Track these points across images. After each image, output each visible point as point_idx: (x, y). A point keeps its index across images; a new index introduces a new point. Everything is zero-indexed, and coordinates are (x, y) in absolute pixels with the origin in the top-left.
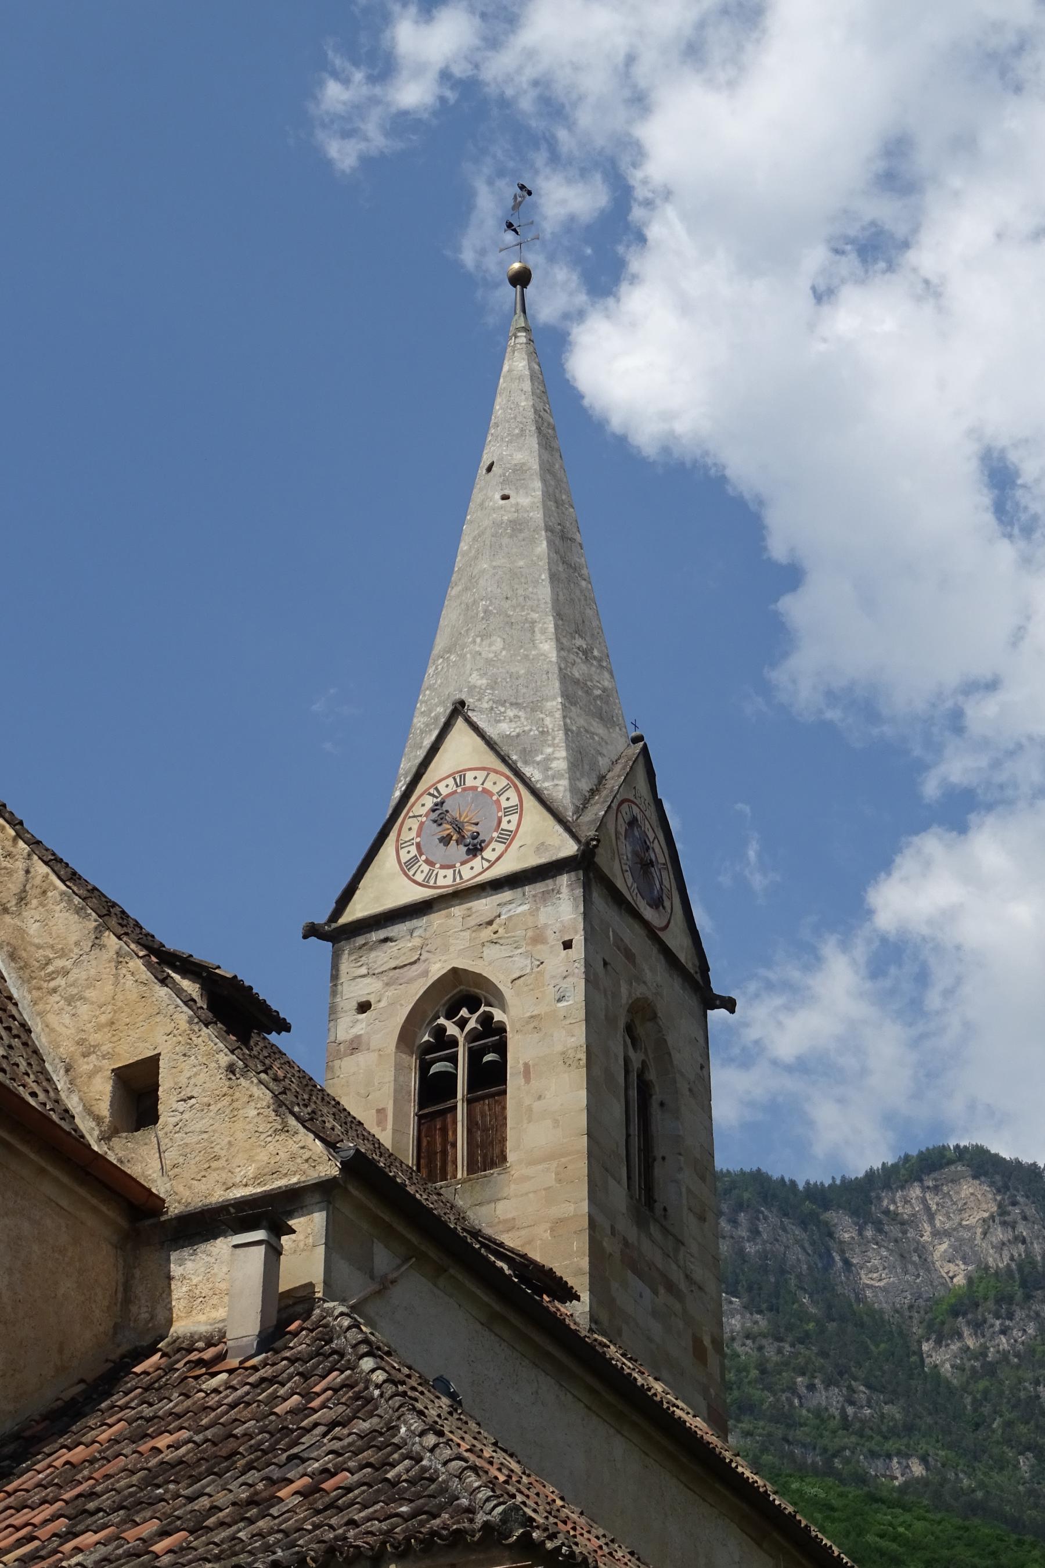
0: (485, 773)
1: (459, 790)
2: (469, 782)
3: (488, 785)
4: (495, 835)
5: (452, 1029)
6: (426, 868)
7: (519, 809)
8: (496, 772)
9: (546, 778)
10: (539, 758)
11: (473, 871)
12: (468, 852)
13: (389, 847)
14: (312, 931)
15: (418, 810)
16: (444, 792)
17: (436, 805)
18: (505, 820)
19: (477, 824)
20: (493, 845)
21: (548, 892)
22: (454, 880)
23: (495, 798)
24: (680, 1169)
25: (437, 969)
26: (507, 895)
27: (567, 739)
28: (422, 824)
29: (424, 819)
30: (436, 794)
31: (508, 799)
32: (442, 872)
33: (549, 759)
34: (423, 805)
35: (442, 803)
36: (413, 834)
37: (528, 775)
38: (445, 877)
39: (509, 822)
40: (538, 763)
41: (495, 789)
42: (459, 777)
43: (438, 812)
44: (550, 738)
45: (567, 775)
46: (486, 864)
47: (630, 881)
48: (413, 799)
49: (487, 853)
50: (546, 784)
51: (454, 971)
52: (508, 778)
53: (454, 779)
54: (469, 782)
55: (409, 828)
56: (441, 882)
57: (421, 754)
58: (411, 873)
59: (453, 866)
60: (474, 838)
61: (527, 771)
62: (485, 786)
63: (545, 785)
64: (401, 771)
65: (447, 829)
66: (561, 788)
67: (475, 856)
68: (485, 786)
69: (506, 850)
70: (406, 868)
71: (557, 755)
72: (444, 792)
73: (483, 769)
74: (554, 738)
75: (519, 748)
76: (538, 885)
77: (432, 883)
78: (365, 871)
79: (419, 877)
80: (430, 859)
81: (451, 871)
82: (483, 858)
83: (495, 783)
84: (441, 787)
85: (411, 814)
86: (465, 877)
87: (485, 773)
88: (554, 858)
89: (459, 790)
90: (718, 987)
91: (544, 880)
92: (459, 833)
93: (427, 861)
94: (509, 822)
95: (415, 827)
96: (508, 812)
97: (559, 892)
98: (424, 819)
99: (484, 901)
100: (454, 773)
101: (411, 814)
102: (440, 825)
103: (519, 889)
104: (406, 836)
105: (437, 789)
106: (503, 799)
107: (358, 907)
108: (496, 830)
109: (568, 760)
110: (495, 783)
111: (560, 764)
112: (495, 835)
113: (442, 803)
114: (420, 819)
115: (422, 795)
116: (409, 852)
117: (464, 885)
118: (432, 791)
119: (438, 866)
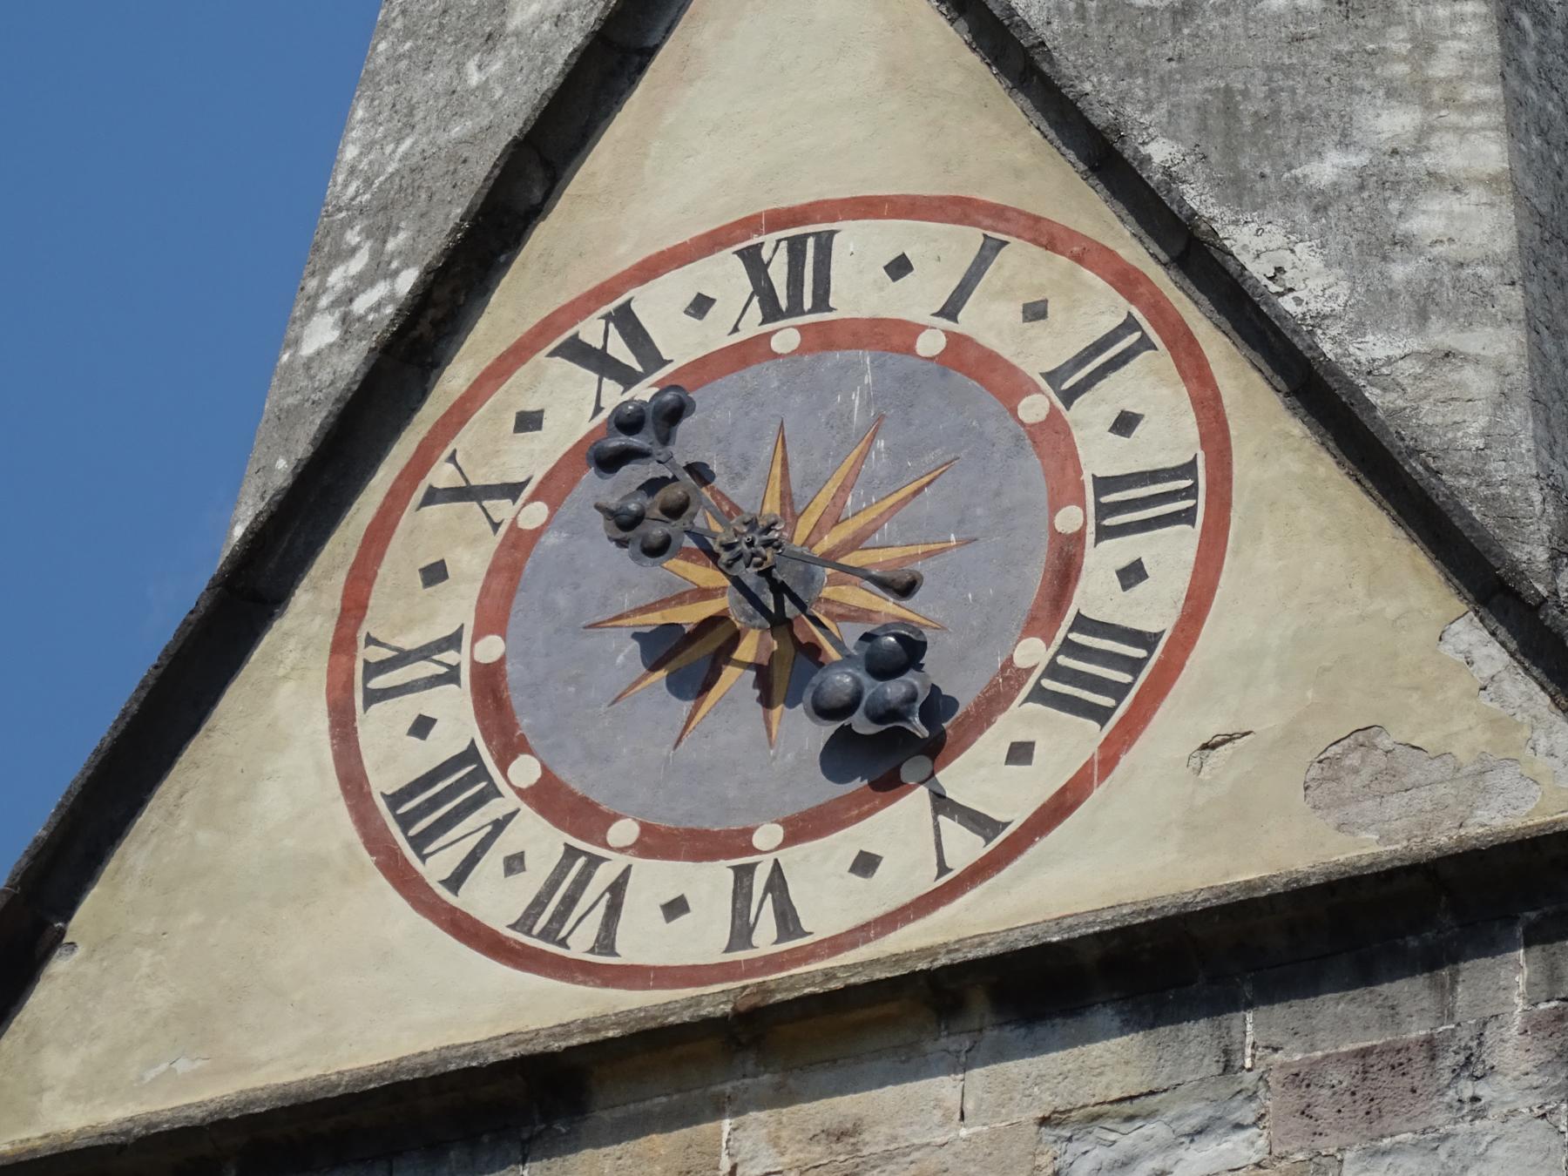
0: (972, 238)
1: (786, 338)
2: (857, 290)
3: (990, 321)
4: (1032, 653)
6: (541, 840)
7: (1196, 496)
8: (1048, 237)
9: (1375, 308)
10: (1328, 168)
11: (871, 886)
12: (843, 755)
13: (282, 684)
15: (490, 449)
16: (680, 341)
17: (628, 422)
18: (1102, 559)
19: (905, 589)
20: (1020, 719)
21: (1397, 1059)
22: (741, 933)
23: (1034, 409)
26: (1107, 1061)
27: (1510, 56)
28: (518, 543)
29: (534, 515)
30: (619, 349)
31: (1125, 423)
32: (655, 879)
33: (1388, 180)
34: (529, 422)
35: (671, 413)
36: (456, 607)
37: (1259, 270)
38: (676, 908)
39: (1132, 574)
40: (1321, 203)
41: (1040, 352)
42: (787, 249)
43: (634, 474)
44: (1398, 40)
45: (1513, 299)
46: (964, 847)
48: (456, 377)
49: (976, 774)
50: (1375, 347)
52: (1126, 281)
53: (753, 261)
54: (857, 290)
55: (428, 561)
56: (644, 939)
57: (503, 90)
58: (435, 868)
59: (733, 844)
60: (883, 669)
61: (1252, 244)
62: (969, 321)
63: (1369, 351)
64: (344, 189)
65: (696, 589)
66: (1478, 382)
67: (889, 785)
68: (969, 321)
69: (1108, 758)
70: (405, 828)
71: (1450, 156)
72: (680, 341)
73: (956, 209)
74: (1425, 47)
75: (1195, 92)
76: (1332, 1008)
77: (580, 943)
78: (135, 805)
79: (495, 899)
80: (575, 780)
81: (720, 873)
82: (941, 803)
83: (1035, 312)
84: (659, 307)
85: (442, 475)
86: (820, 921)
87: (972, 238)
88: (1444, 837)
89: (786, 338)
91: (1366, 975)
92: (778, 623)
93: (548, 797)
94: (1132, 574)
95: (471, 562)
96: (1125, 504)
97: (1469, 1066)
98: (534, 515)
99: (944, 1088)
100: (750, 224)
101: (442, 475)
102: (658, 550)
103: (1197, 1032)
104: (403, 616)
105: (626, 320)
106: (1089, 419)
107: (58, 1065)
108: (1044, 618)
109: (1520, 198)
110: (1035, 312)
111: (1468, 223)
112: (1032, 653)
113: (671, 413)
114: (503, 509)
115: (519, 353)
116: (422, 727)
117: (808, 976)
118: (591, 330)
119: (624, 832)
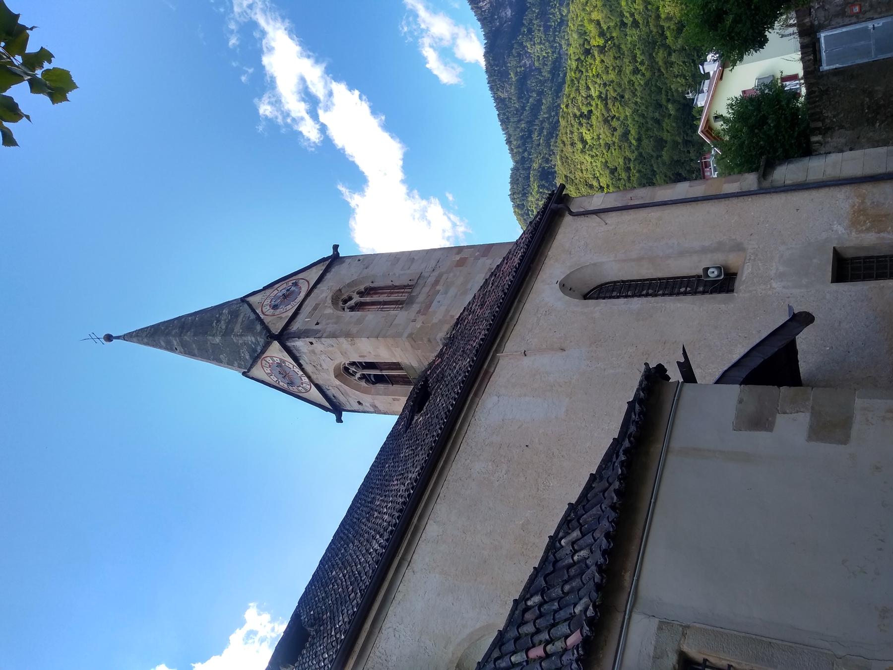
5: (358, 375)
14: (339, 420)
24: (394, 274)
25: (337, 382)
47: (290, 306)
51: (336, 377)
90: (330, 253)
